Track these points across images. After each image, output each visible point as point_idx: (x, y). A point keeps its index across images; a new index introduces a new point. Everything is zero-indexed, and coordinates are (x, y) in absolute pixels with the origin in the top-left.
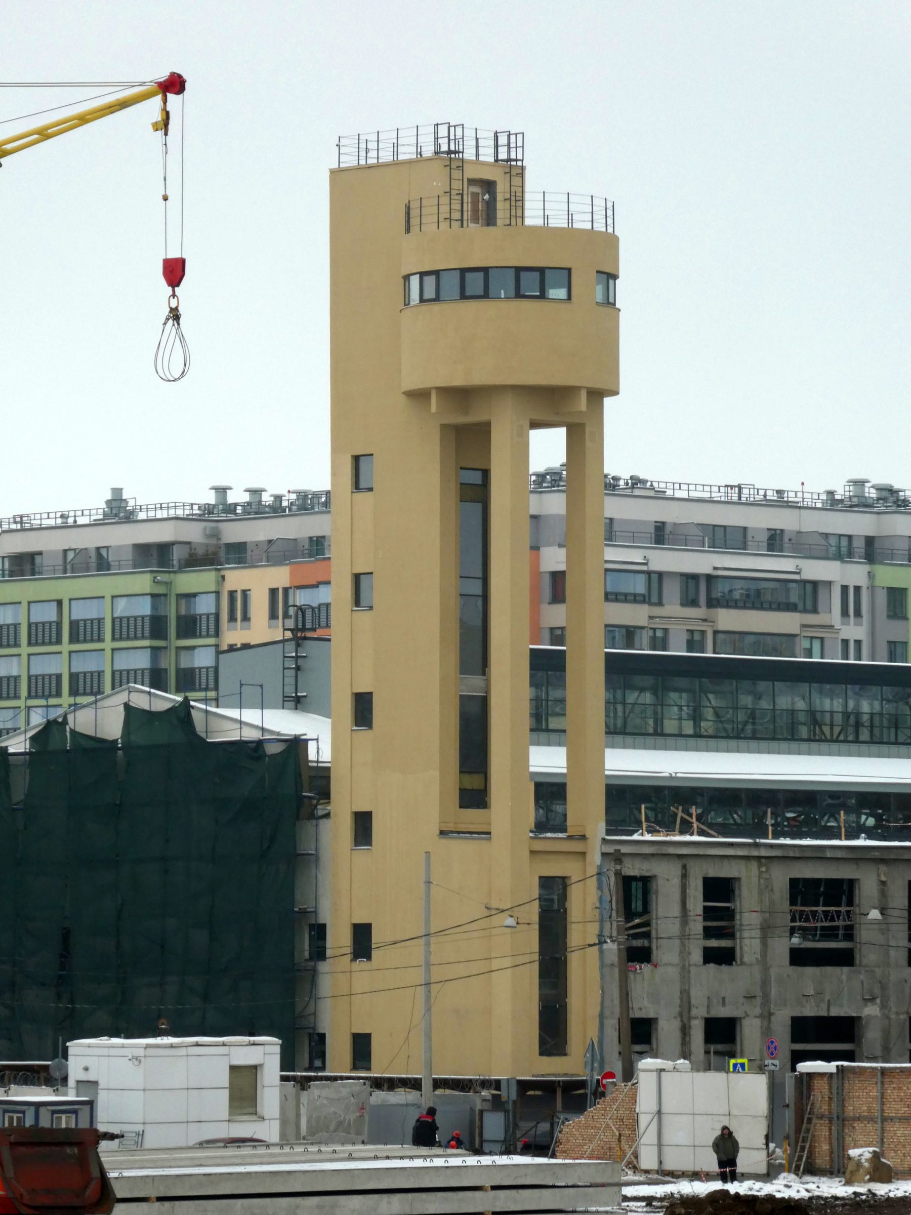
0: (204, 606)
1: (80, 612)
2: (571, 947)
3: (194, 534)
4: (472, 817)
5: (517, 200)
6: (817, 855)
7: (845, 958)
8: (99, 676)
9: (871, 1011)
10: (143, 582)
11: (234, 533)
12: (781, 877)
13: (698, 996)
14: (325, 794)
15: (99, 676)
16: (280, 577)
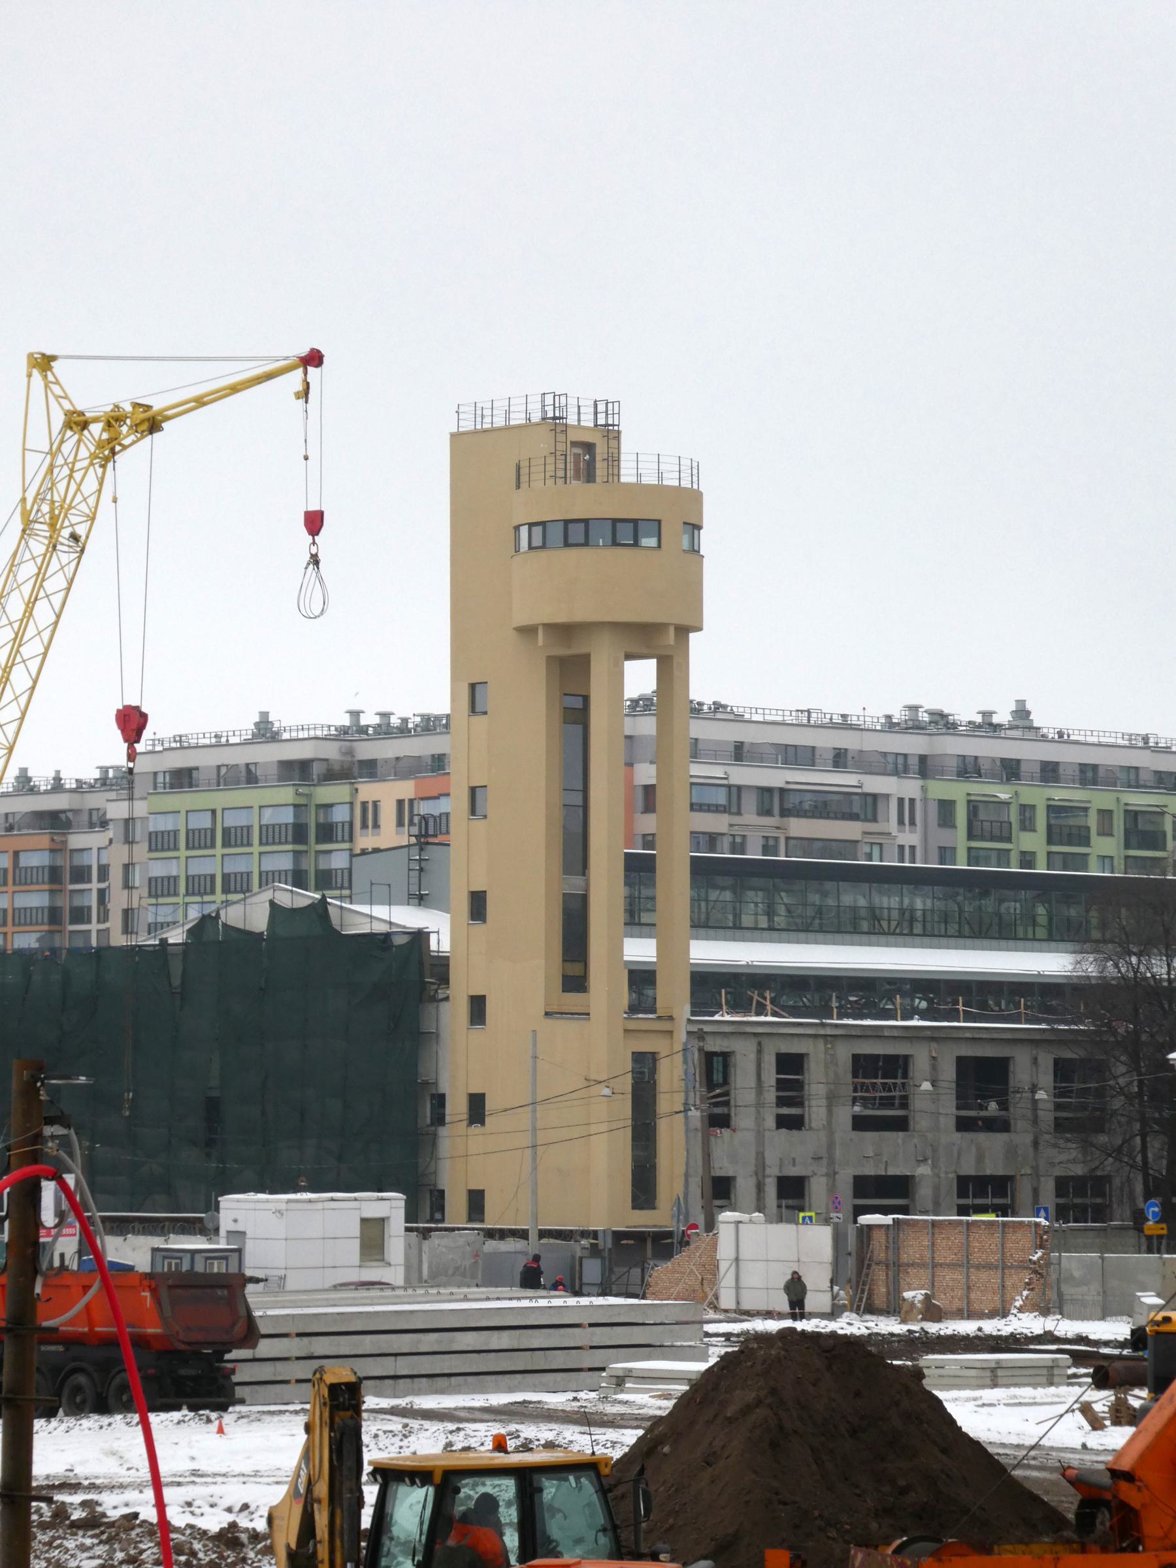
0: (340, 815)
3: (331, 751)
4: (573, 1000)
5: (614, 461)
6: (876, 1034)
7: (901, 1125)
9: (923, 1170)
10: (286, 794)
11: (366, 751)
12: (844, 1053)
13: (771, 1157)
14: (444, 980)
16: (406, 789)
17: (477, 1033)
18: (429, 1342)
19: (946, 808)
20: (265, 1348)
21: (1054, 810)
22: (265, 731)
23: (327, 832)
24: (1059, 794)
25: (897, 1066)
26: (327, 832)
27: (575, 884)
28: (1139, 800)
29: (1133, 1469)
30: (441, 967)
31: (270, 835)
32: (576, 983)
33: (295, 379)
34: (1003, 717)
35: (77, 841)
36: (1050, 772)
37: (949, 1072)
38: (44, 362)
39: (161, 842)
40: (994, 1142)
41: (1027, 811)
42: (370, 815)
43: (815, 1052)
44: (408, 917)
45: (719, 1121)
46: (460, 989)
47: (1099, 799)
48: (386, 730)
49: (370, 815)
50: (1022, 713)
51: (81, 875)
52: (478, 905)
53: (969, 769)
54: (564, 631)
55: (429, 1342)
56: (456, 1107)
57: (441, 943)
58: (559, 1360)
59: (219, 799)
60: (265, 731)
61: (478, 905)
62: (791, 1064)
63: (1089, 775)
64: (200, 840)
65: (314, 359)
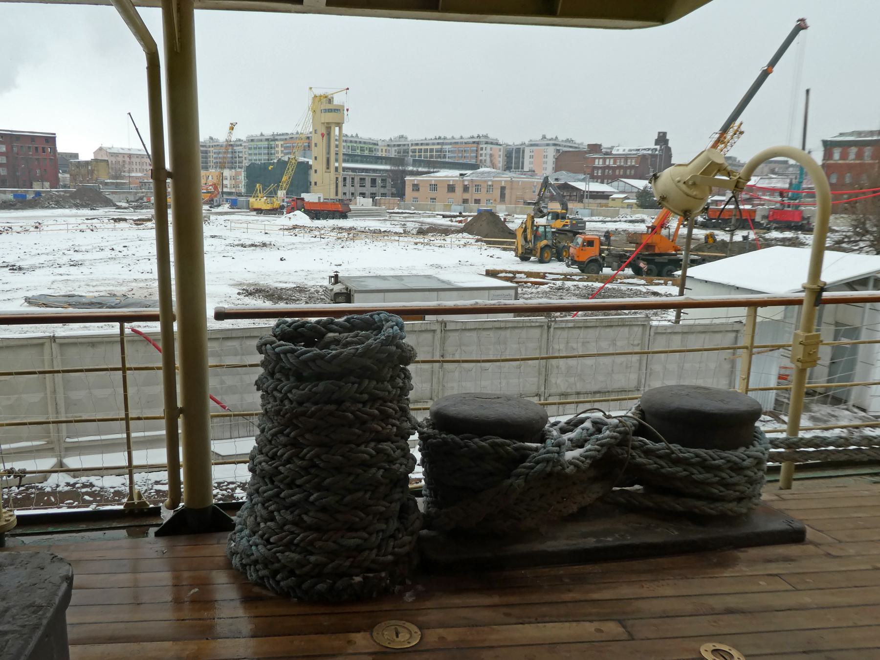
0: (273, 146)
1: (260, 146)
2: (681, 190)
3: (272, 137)
4: (328, 170)
5: (333, 101)
6: (362, 175)
7: (364, 186)
8: (517, 158)
9: (367, 192)
10: (266, 143)
11: (276, 137)
12: (359, 177)
13: (351, 190)
14: (311, 168)
15: (517, 158)
16: (282, 143)
17: (316, 174)
18: (359, 212)
19: (349, 146)
20: (352, 212)
21: (361, 147)
22: (262, 135)
23: (271, 148)
24: (362, 145)
25: (364, 179)
26: (271, 148)
27: (328, 156)
28: (371, 146)
29: (516, 230)
30: (311, 167)
31: (264, 148)
32: (328, 168)
33: (345, 91)
34: (354, 135)
35: (235, 148)
36: (360, 142)
37: (370, 180)
38: (311, 88)
39: (250, 149)
40: (374, 188)
41: (358, 147)
42: (277, 146)
43: (348, 177)
44: (306, 160)
45: (345, 185)
46: (314, 168)
47: (366, 146)
48: (277, 135)
49: (277, 146)
50: (556, 137)
51: (235, 152)
52: (316, 158)
53: (351, 142)
54: (328, 123)
55: (359, 212)
56: (313, 183)
57: (311, 163)
58: (372, 214)
59: (258, 143)
60: (262, 135)
61: (316, 158)
62: (353, 179)
63: (365, 143)
64: (255, 148)
65: (348, 89)
